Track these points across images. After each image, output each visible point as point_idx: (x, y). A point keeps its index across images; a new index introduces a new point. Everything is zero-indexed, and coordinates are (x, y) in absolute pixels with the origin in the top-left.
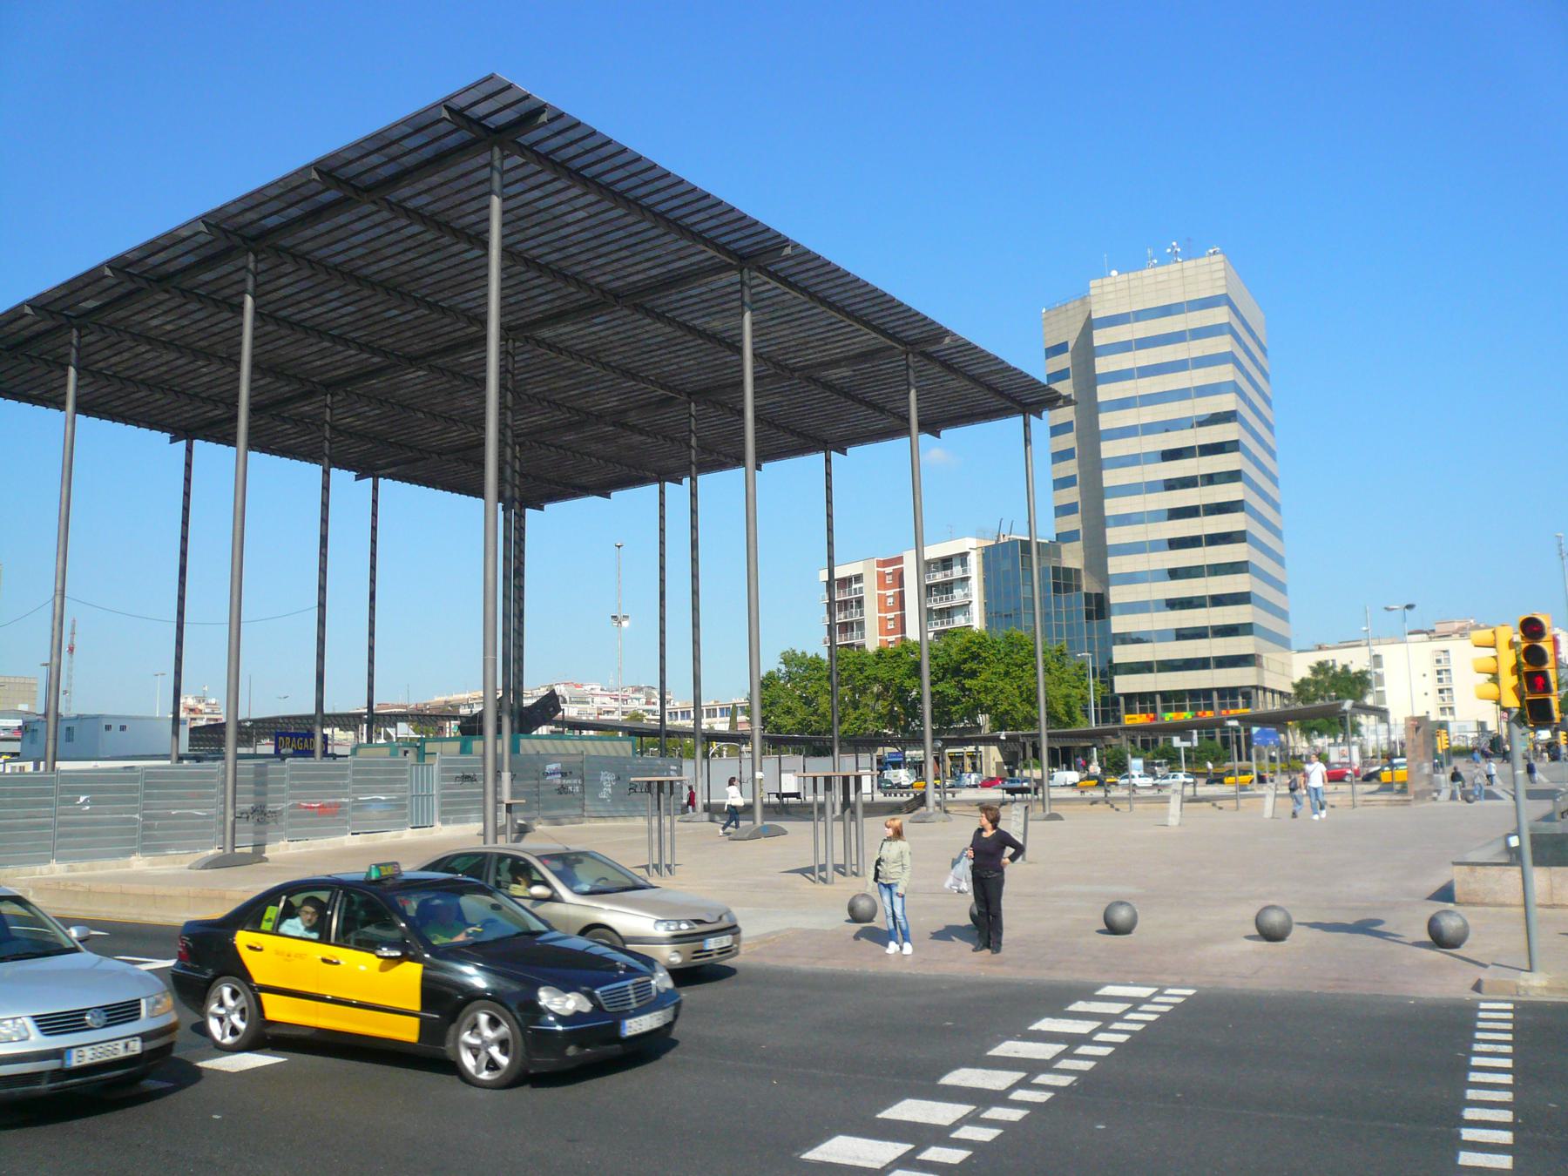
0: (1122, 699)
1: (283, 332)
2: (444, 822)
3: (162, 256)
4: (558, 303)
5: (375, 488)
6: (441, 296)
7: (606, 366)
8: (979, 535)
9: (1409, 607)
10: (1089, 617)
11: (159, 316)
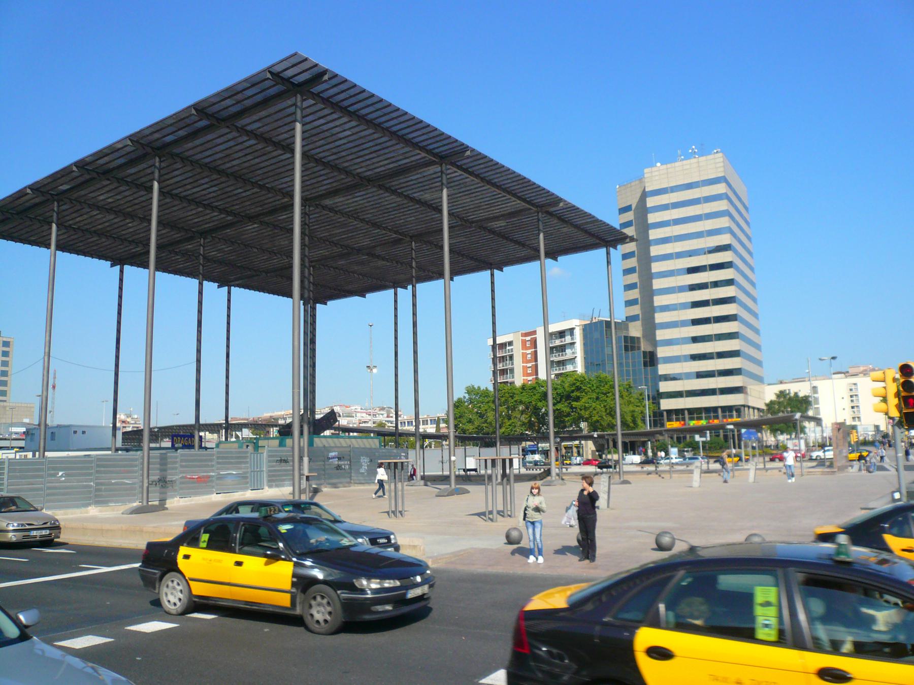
0: (665, 413)
1: (177, 202)
2: (270, 486)
3: (106, 159)
4: (334, 184)
5: (229, 293)
6: (267, 181)
7: (362, 220)
8: (581, 318)
9: (834, 358)
10: (645, 365)
11: (104, 194)
